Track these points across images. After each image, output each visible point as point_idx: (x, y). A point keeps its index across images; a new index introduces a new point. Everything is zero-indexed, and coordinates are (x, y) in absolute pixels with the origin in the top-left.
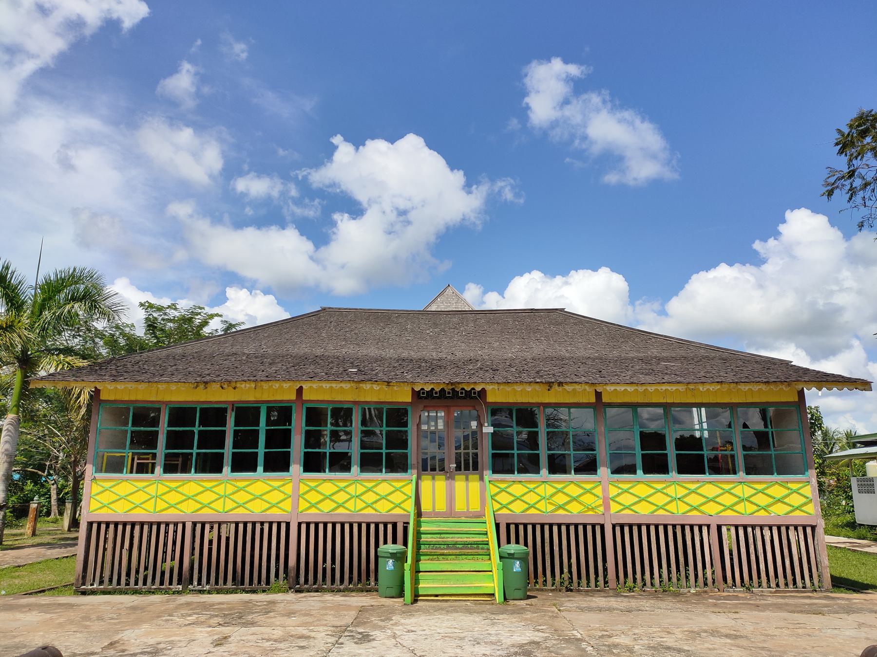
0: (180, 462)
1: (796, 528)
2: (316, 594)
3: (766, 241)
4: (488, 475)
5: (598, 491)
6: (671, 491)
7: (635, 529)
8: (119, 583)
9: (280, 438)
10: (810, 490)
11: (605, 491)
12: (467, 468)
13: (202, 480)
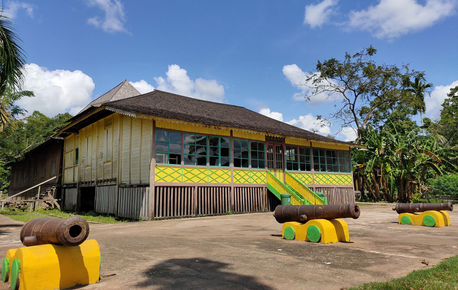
0: (177, 159)
1: (260, 188)
2: (216, 217)
3: (158, 77)
4: (286, 170)
5: (229, 173)
6: (180, 171)
7: (248, 189)
8: (166, 215)
9: (225, 152)
10: (351, 177)
11: (313, 177)
12: (279, 168)
13: (200, 168)
